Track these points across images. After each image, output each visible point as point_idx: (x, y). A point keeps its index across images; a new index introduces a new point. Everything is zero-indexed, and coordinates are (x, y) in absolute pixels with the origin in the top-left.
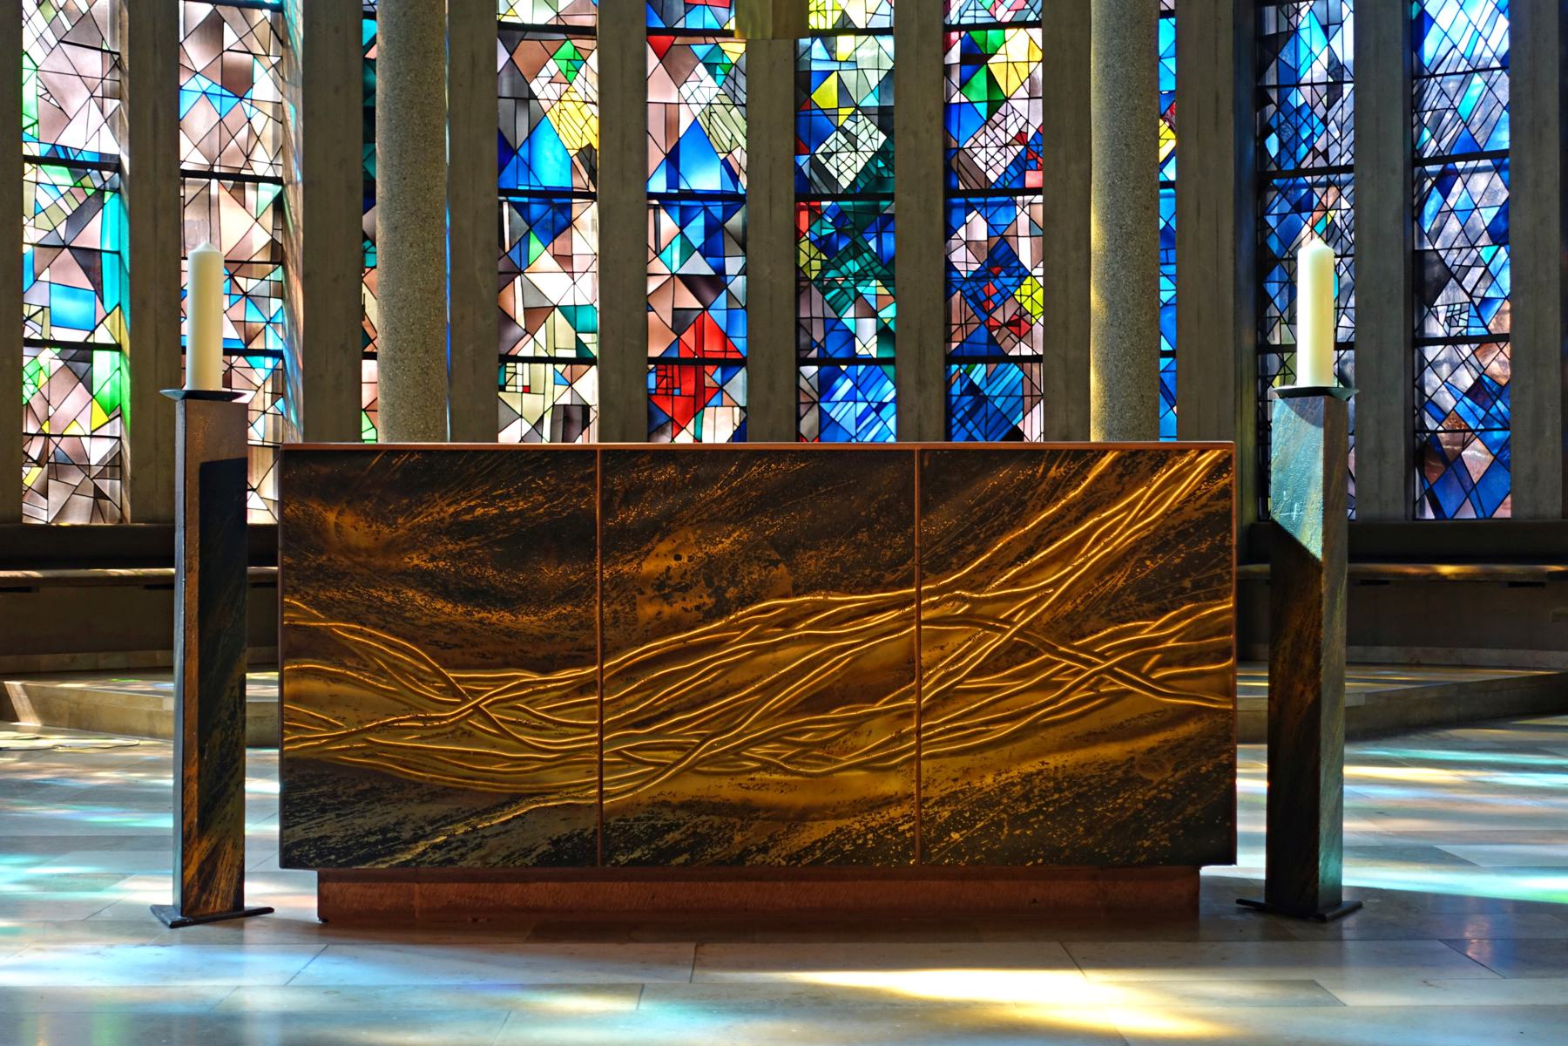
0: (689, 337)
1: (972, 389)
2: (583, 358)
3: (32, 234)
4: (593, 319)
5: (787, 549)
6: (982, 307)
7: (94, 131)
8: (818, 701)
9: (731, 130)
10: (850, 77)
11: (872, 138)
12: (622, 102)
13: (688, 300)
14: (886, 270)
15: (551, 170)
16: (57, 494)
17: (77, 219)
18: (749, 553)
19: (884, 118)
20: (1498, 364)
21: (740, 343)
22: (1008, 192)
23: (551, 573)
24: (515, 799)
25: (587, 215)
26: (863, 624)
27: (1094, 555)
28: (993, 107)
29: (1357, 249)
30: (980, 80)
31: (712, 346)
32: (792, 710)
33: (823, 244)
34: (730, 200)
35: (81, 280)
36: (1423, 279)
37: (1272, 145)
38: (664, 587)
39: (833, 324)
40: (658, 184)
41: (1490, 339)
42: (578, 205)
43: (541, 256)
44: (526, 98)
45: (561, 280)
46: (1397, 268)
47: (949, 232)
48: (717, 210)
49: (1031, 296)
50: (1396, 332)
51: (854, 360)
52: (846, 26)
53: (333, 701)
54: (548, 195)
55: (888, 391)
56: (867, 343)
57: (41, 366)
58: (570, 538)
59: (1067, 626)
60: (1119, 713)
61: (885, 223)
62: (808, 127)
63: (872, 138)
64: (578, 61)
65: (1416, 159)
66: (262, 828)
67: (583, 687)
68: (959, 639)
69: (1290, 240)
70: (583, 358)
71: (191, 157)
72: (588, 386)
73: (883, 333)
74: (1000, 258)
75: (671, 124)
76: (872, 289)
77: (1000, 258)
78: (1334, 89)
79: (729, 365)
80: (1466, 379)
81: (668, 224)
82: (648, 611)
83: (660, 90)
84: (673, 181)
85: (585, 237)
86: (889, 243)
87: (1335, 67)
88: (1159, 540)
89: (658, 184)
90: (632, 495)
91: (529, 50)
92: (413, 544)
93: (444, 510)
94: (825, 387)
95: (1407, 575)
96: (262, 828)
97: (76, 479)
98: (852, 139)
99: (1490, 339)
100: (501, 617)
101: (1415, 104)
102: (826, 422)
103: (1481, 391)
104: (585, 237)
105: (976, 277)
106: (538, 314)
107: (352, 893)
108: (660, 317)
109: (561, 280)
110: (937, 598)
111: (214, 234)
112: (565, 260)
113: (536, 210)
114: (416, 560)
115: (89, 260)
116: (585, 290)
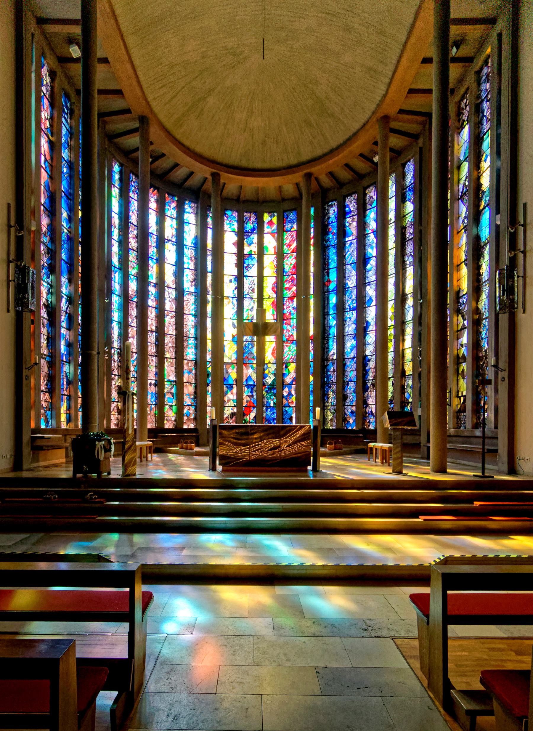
0: (249, 404)
1: (286, 411)
2: (235, 406)
3: (165, 391)
4: (235, 401)
5: (268, 435)
6: (287, 400)
7: (173, 378)
8: (271, 450)
9: (254, 377)
10: (270, 369)
11: (273, 377)
12: (240, 373)
13: (249, 399)
14: (275, 395)
15: (230, 382)
16: (168, 424)
17: (171, 389)
18: (264, 435)
19: (274, 375)
20: (354, 409)
21: (255, 404)
22: (290, 385)
23: (245, 437)
24: (241, 459)
25: (235, 387)
26: (275, 442)
27: (297, 436)
28: (289, 373)
29: (337, 393)
30: (287, 370)
31: (252, 405)
32: (268, 451)
33: (267, 392)
34: (254, 385)
35: (171, 397)
36: (345, 397)
37: (326, 379)
38: (256, 439)
39: (267, 402)
40: (245, 383)
41: (353, 406)
42: (234, 386)
43: (229, 393)
44: (227, 372)
45: (231, 396)
46: (341, 396)
47: (283, 390)
48: (252, 387)
49: (294, 399)
50: (341, 405)
51: (270, 407)
52: (269, 362)
53: (224, 450)
54: (230, 385)
55: (275, 411)
56: (272, 405)
57: (167, 407)
58: (247, 434)
59: (295, 443)
60: (300, 451)
61: (274, 389)
62: (264, 376)
63: (273, 377)
64: (234, 368)
65: (344, 382)
66: (218, 462)
67: (248, 448)
68: (284, 444)
69: (328, 391)
70: (235, 406)
71: (185, 381)
72: (235, 410)
73: (274, 403)
74: (290, 394)
75: (246, 376)
76: (273, 397)
77: (290, 394)
78: (334, 372)
79: (254, 407)
80: (350, 411)
81: (246, 389)
82: (254, 441)
83: (245, 371)
84: (247, 383)
85: (235, 390)
86: (275, 391)
87: (334, 369)
88: (303, 435)
89: (245, 383)
90: (253, 430)
91: (228, 366)
92: (232, 434)
93: (234, 431)
94: (267, 410)
95: (62, 488)
96: (218, 462)
97: (171, 422)
98: (270, 377)
99: (353, 406)
100: (240, 441)
101: (344, 375)
102: (266, 415)
103: (352, 412)
104: (235, 390)
105: (287, 396)
106: (229, 401)
107: (226, 468)
108: (245, 401)
109: (231, 396)
110: (282, 440)
111: (188, 390)
112: (232, 393)
113: (229, 386)
114: (232, 436)
115: (172, 394)
116: (235, 397)
